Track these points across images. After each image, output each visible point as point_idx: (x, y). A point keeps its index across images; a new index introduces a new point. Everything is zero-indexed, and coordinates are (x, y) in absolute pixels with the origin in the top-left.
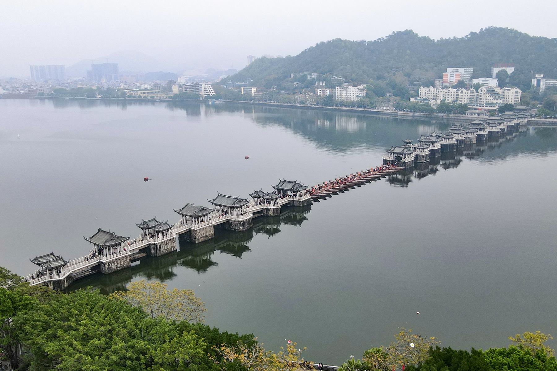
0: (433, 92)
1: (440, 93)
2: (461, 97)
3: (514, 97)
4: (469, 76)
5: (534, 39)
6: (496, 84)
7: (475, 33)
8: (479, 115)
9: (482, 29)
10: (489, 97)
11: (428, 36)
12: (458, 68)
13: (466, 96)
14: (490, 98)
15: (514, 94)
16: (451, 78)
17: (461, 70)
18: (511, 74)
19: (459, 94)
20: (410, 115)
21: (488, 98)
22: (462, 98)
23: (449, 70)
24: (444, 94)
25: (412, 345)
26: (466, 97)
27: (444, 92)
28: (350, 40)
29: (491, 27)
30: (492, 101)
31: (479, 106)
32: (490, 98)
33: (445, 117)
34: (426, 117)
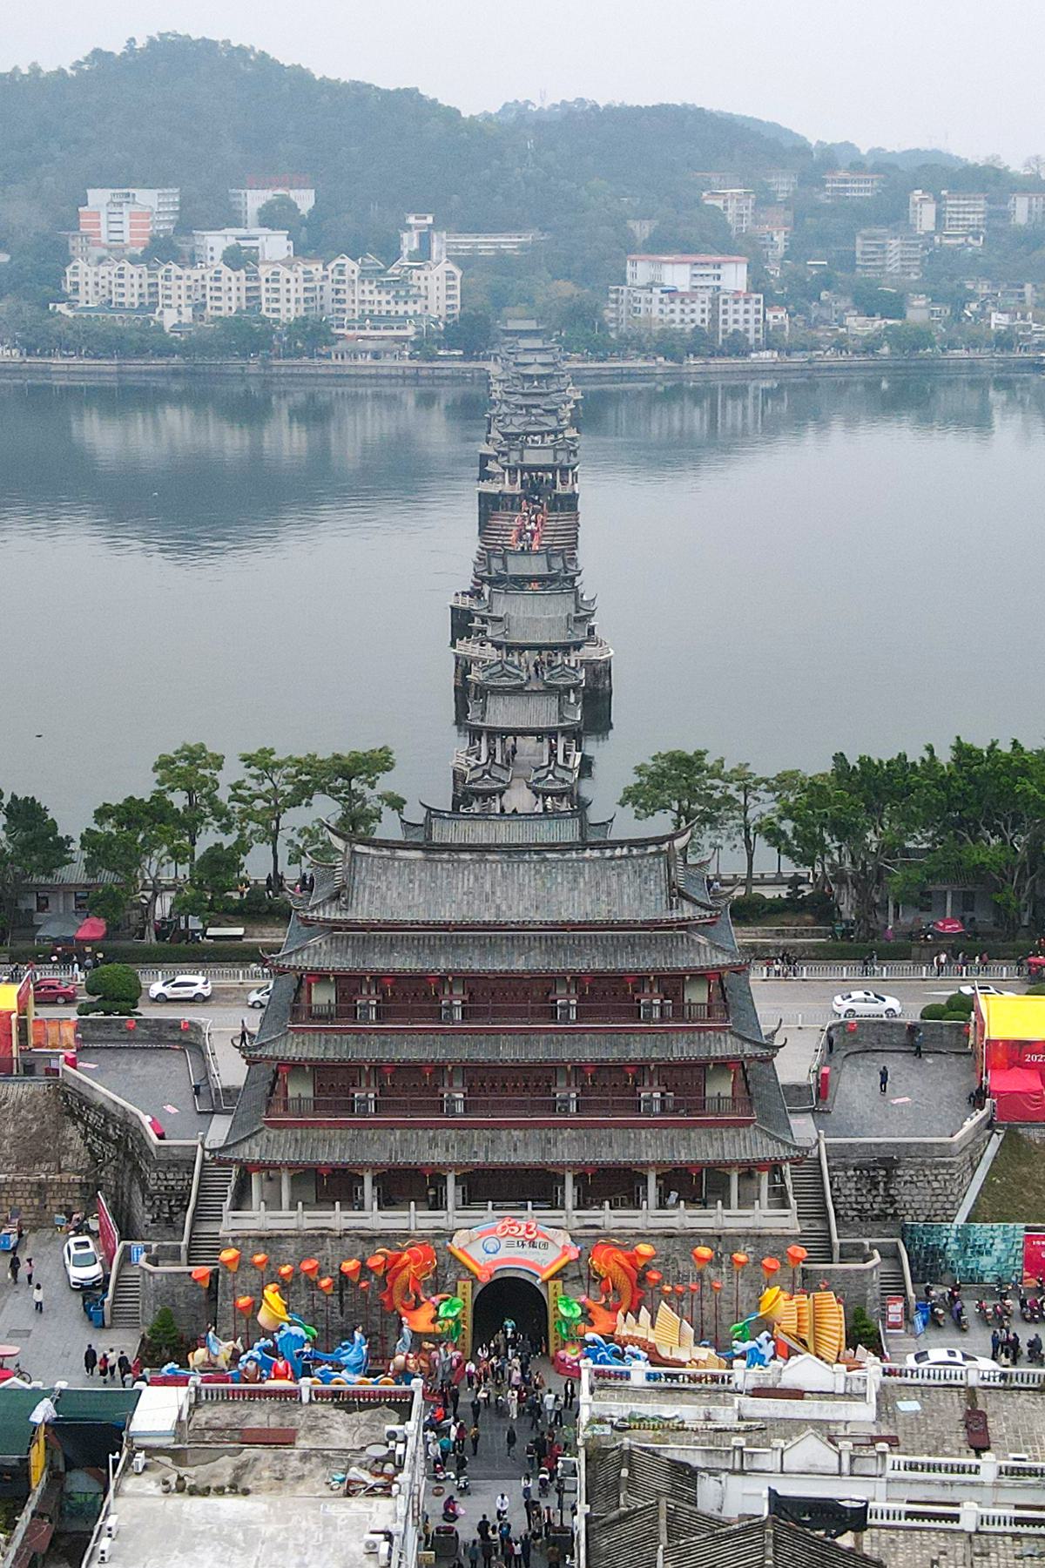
0: (136, 281)
1: (174, 283)
2: (275, 296)
3: (443, 293)
4: (171, 222)
5: (331, 88)
6: (288, 248)
7: (111, 54)
8: (376, 356)
9: (133, 40)
12: (132, 191)
14: (376, 297)
15: (443, 284)
17: (147, 198)
18: (311, 212)
19: (161, 282)
20: (108, 369)
21: (368, 297)
22: (277, 300)
23: (98, 197)
24: (189, 288)
26: (293, 296)
27: (189, 278)
29: (168, 33)
30: (388, 308)
31: (349, 328)
32: (376, 297)
33: (253, 369)
34: (176, 374)
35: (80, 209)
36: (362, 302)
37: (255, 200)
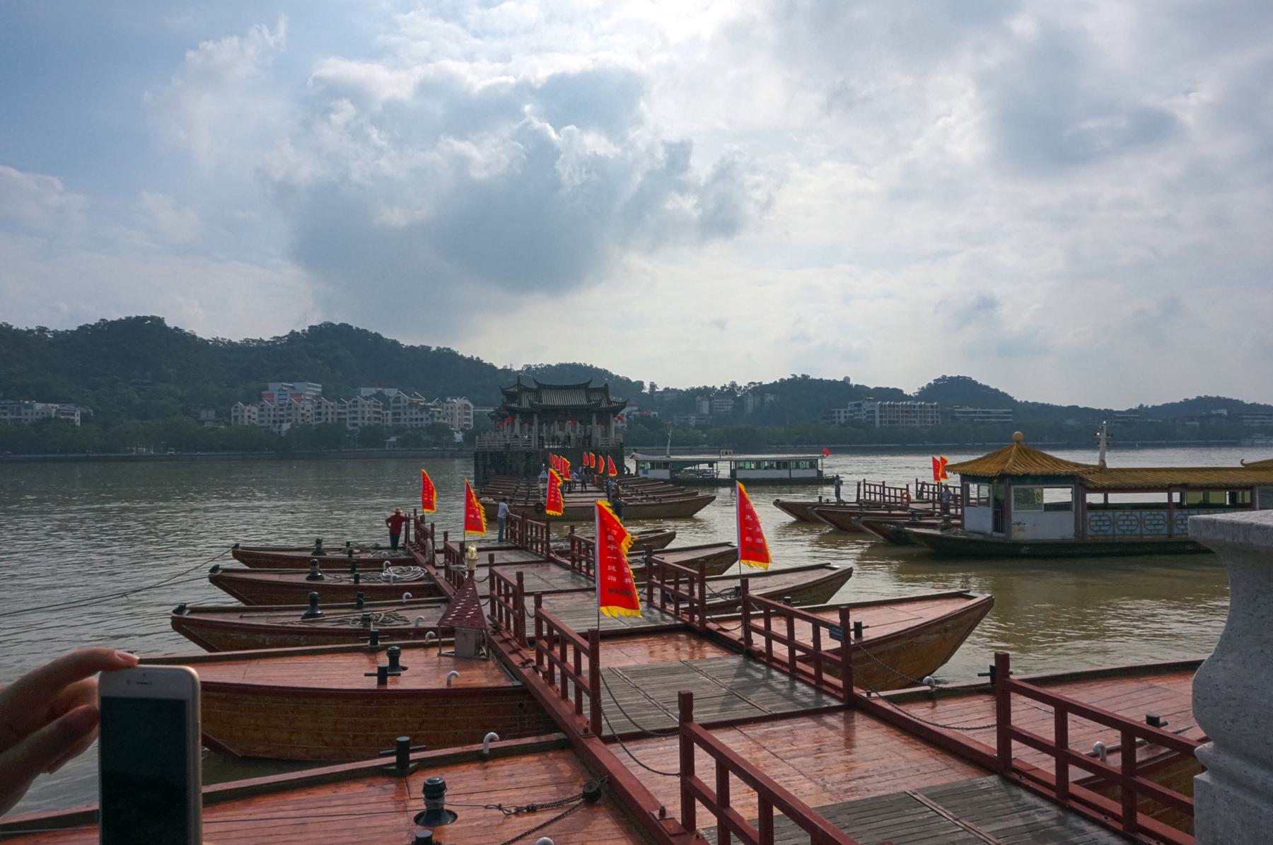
10: (416, 413)
11: (780, 378)
13: (272, 416)
16: (281, 397)
21: (414, 416)
25: (1105, 422)
28: (12, 326)
32: (419, 416)
35: (263, 393)
36: (411, 419)
37: (366, 391)
